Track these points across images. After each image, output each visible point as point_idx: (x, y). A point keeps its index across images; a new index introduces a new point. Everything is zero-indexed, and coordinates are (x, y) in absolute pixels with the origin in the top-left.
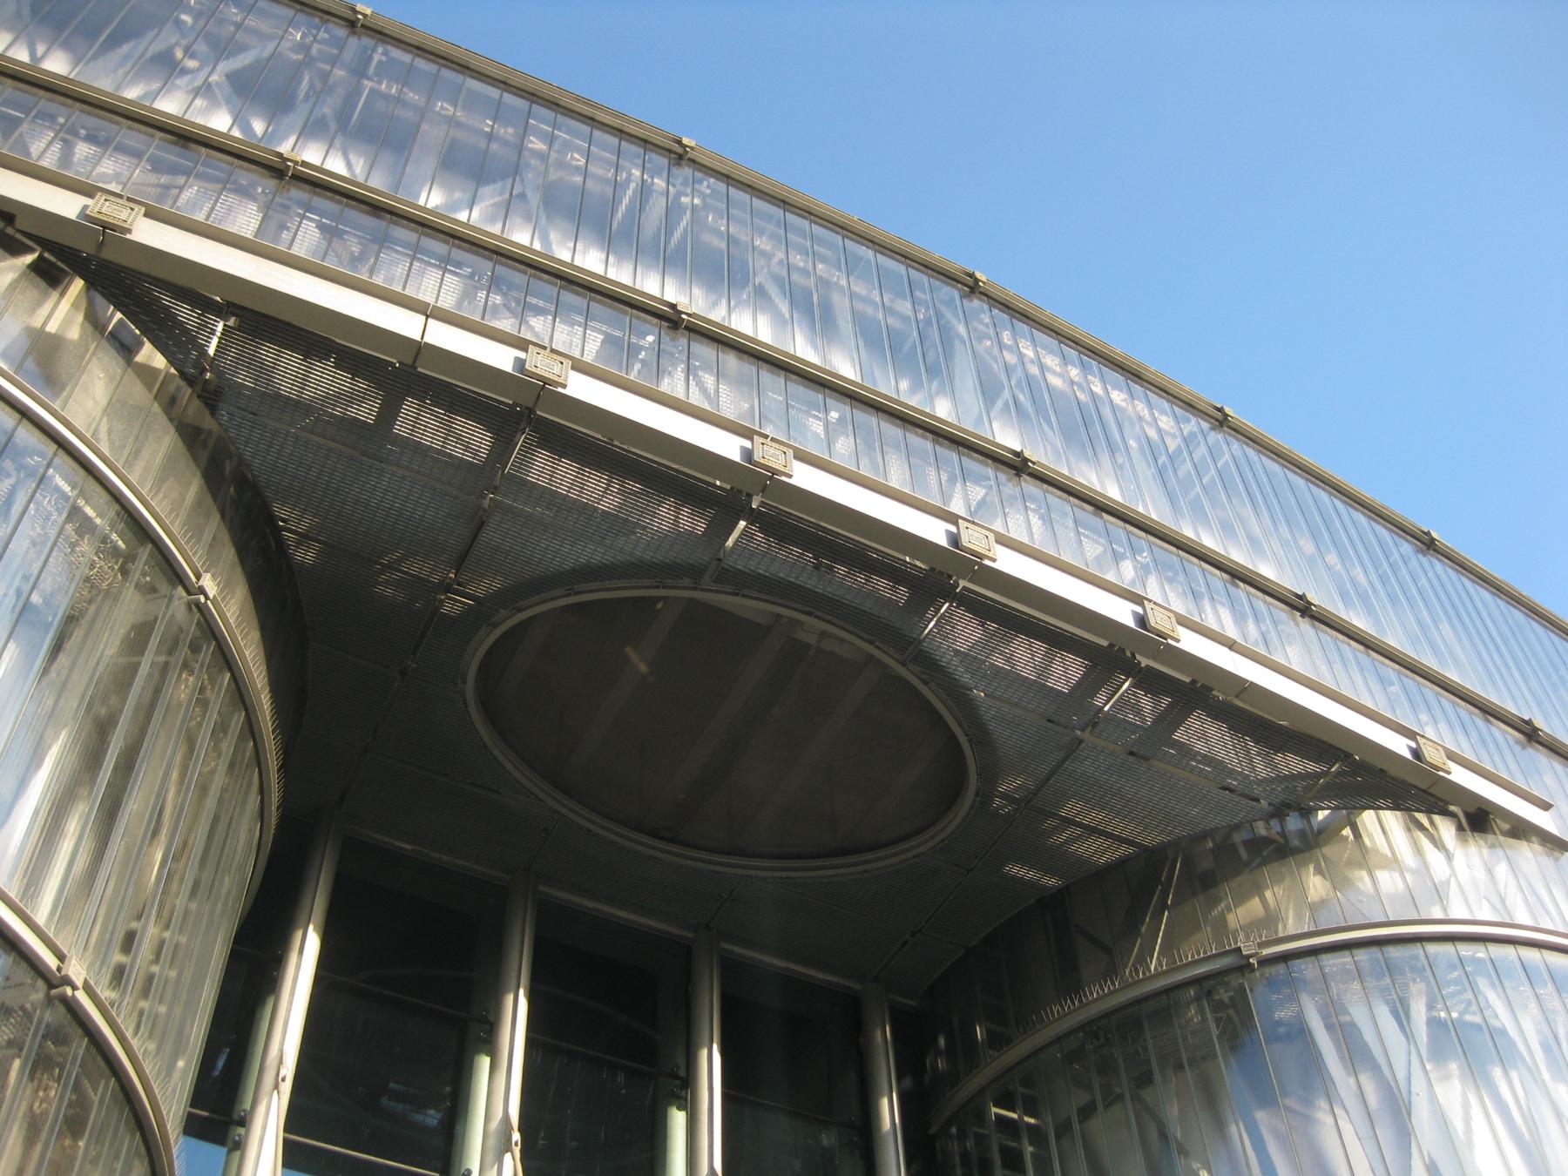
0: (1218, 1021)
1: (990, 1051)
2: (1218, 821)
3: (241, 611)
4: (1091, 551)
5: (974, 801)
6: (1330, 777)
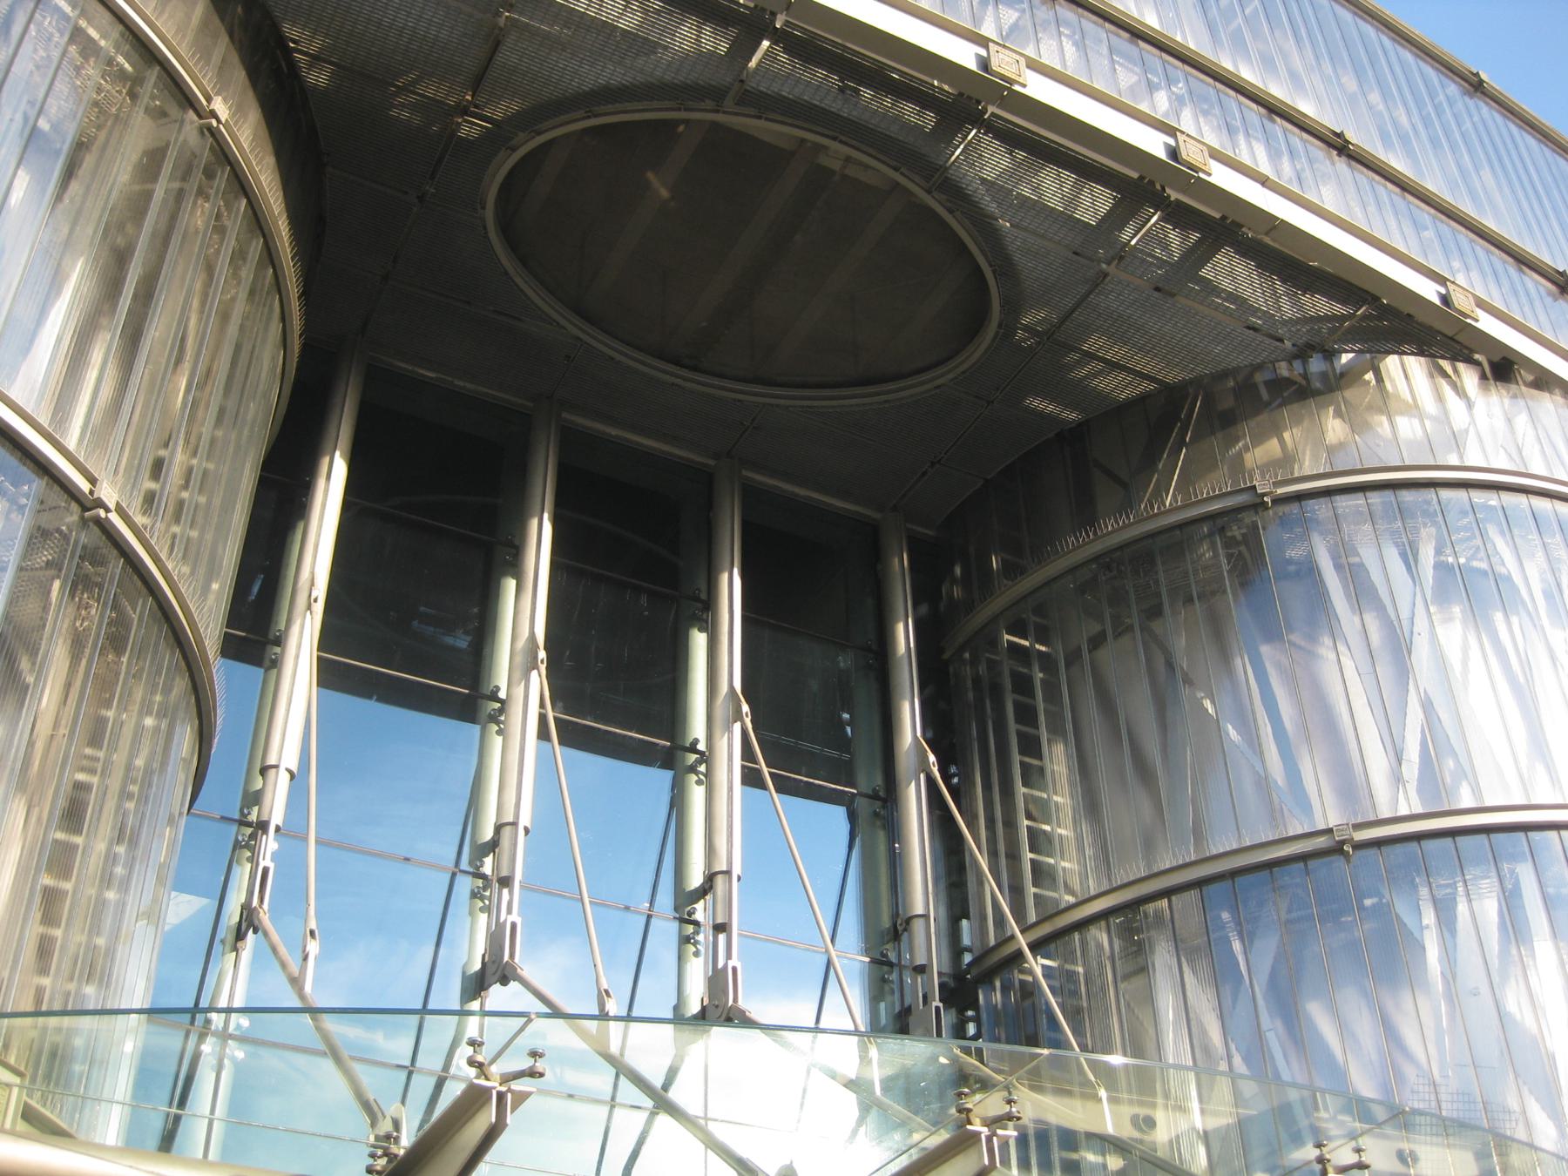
0: (1229, 557)
1: (1005, 581)
2: (1241, 360)
3: (254, 135)
4: (1125, 80)
5: (997, 333)
6: (1356, 319)
